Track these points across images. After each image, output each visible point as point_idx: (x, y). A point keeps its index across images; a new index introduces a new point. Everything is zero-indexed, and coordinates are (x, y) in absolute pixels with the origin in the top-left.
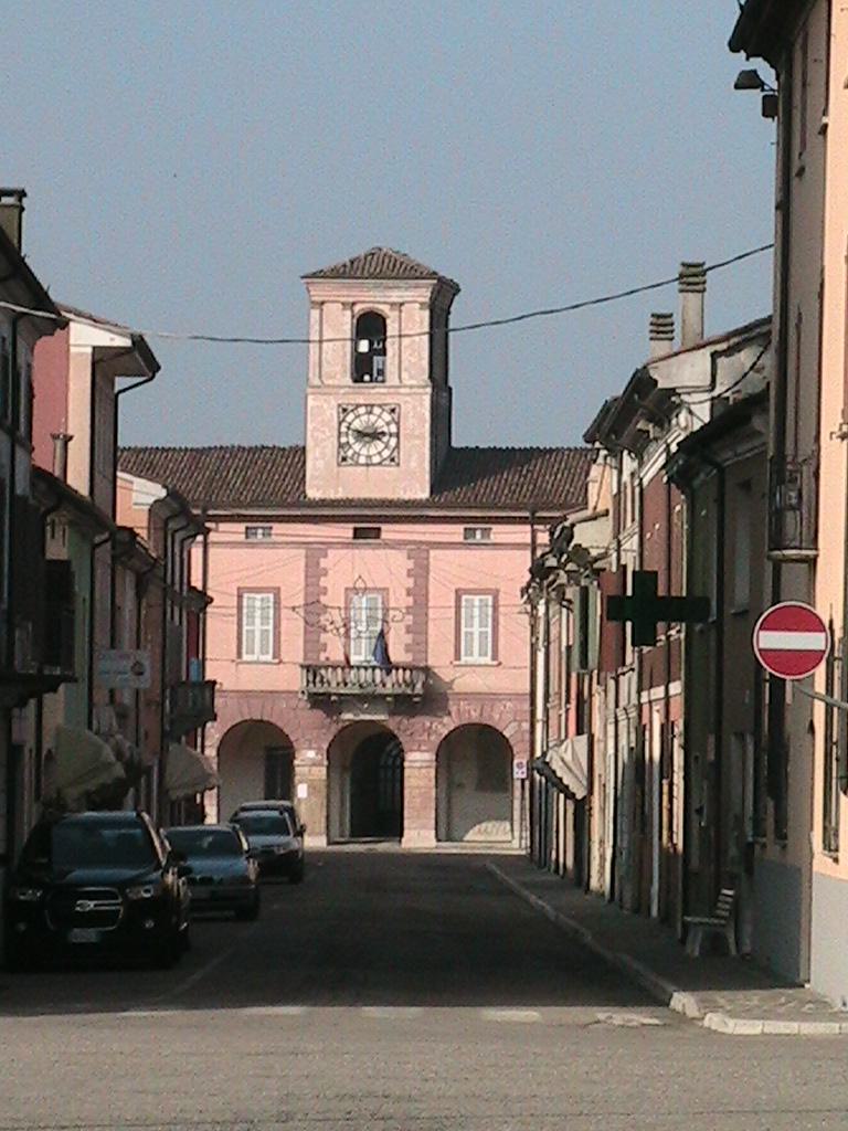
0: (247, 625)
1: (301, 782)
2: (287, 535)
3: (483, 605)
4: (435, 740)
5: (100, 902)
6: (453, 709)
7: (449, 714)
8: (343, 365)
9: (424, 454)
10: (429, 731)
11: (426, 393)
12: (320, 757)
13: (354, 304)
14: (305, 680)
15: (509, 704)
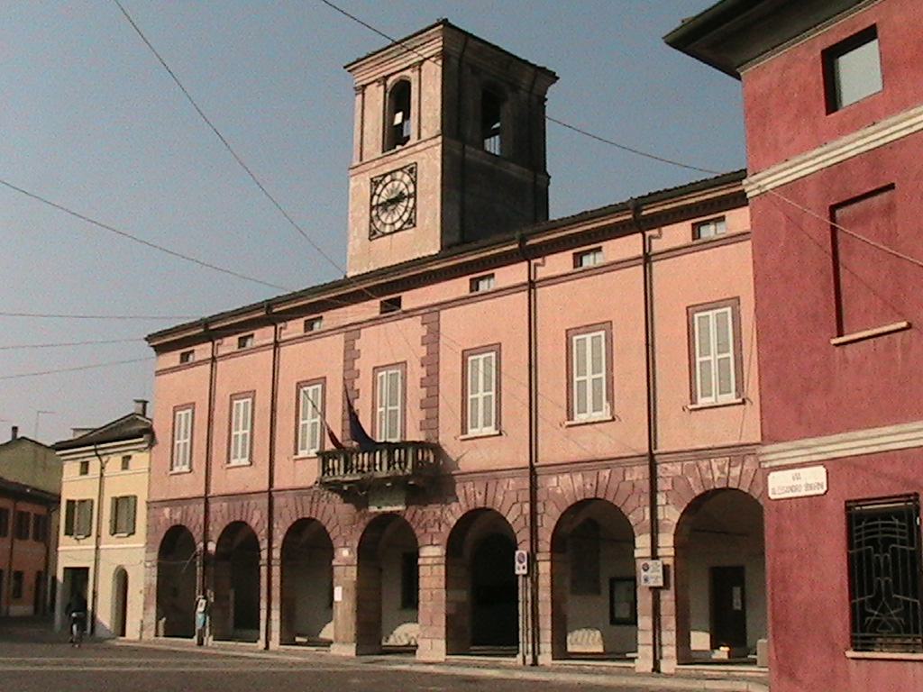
0: (729, 358)
1: (337, 585)
2: (388, 317)
3: (720, 321)
4: (446, 531)
5: (672, 572)
6: (460, 492)
7: (457, 500)
8: (377, 139)
9: (436, 209)
10: (439, 522)
11: (437, 145)
12: (352, 555)
13: (386, 78)
14: (321, 471)
15: (512, 482)
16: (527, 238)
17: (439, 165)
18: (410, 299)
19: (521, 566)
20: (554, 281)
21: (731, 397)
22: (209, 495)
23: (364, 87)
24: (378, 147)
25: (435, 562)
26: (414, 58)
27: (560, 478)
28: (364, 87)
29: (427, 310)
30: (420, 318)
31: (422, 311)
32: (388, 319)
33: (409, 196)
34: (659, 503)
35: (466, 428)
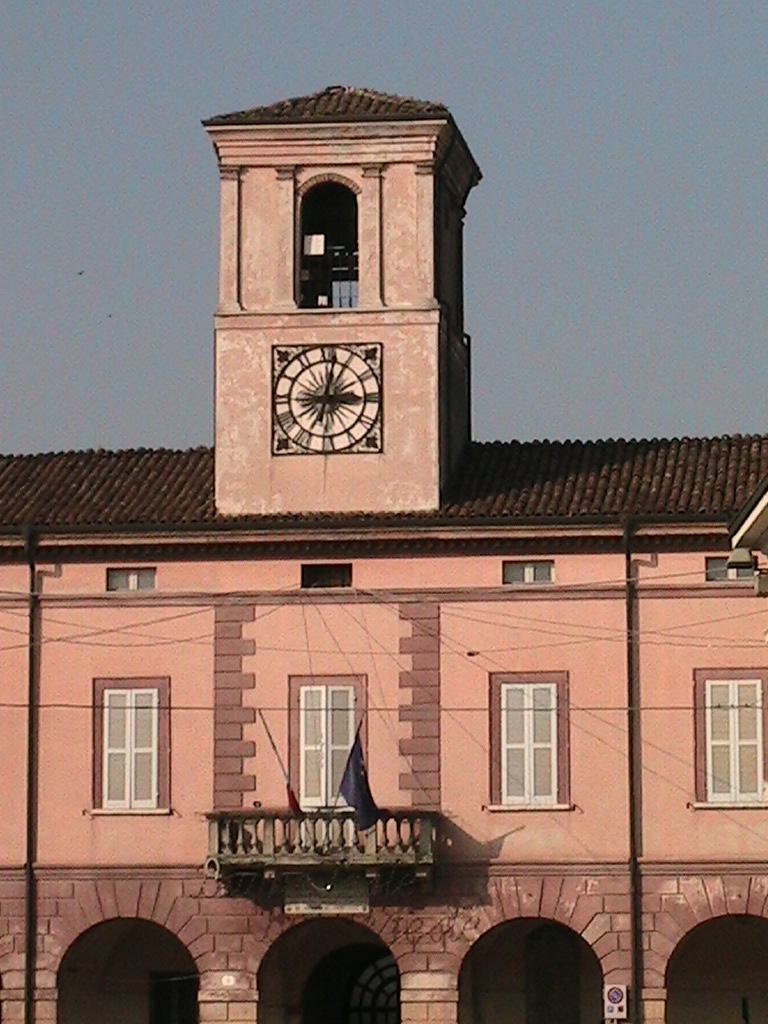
0: (150, 754)
4: (457, 949)
16: (42, 536)
17: (433, 360)
18: (368, 573)
19: (616, 1006)
20: (668, 593)
21: (150, 805)
22: (34, 865)
23: (242, 169)
24: (286, 291)
25: (436, 998)
26: (371, 152)
27: (682, 882)
28: (385, 165)
29: (413, 598)
30: (397, 606)
31: (404, 599)
32: (327, 599)
33: (367, 398)
34: (644, 928)
35: (101, 798)
